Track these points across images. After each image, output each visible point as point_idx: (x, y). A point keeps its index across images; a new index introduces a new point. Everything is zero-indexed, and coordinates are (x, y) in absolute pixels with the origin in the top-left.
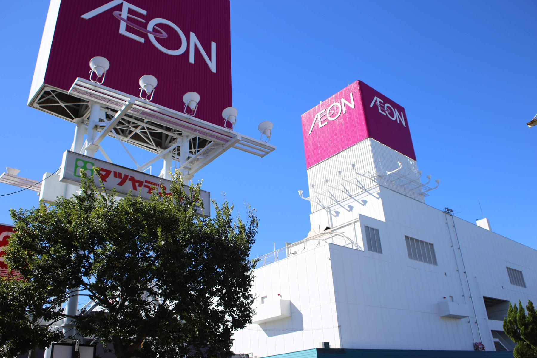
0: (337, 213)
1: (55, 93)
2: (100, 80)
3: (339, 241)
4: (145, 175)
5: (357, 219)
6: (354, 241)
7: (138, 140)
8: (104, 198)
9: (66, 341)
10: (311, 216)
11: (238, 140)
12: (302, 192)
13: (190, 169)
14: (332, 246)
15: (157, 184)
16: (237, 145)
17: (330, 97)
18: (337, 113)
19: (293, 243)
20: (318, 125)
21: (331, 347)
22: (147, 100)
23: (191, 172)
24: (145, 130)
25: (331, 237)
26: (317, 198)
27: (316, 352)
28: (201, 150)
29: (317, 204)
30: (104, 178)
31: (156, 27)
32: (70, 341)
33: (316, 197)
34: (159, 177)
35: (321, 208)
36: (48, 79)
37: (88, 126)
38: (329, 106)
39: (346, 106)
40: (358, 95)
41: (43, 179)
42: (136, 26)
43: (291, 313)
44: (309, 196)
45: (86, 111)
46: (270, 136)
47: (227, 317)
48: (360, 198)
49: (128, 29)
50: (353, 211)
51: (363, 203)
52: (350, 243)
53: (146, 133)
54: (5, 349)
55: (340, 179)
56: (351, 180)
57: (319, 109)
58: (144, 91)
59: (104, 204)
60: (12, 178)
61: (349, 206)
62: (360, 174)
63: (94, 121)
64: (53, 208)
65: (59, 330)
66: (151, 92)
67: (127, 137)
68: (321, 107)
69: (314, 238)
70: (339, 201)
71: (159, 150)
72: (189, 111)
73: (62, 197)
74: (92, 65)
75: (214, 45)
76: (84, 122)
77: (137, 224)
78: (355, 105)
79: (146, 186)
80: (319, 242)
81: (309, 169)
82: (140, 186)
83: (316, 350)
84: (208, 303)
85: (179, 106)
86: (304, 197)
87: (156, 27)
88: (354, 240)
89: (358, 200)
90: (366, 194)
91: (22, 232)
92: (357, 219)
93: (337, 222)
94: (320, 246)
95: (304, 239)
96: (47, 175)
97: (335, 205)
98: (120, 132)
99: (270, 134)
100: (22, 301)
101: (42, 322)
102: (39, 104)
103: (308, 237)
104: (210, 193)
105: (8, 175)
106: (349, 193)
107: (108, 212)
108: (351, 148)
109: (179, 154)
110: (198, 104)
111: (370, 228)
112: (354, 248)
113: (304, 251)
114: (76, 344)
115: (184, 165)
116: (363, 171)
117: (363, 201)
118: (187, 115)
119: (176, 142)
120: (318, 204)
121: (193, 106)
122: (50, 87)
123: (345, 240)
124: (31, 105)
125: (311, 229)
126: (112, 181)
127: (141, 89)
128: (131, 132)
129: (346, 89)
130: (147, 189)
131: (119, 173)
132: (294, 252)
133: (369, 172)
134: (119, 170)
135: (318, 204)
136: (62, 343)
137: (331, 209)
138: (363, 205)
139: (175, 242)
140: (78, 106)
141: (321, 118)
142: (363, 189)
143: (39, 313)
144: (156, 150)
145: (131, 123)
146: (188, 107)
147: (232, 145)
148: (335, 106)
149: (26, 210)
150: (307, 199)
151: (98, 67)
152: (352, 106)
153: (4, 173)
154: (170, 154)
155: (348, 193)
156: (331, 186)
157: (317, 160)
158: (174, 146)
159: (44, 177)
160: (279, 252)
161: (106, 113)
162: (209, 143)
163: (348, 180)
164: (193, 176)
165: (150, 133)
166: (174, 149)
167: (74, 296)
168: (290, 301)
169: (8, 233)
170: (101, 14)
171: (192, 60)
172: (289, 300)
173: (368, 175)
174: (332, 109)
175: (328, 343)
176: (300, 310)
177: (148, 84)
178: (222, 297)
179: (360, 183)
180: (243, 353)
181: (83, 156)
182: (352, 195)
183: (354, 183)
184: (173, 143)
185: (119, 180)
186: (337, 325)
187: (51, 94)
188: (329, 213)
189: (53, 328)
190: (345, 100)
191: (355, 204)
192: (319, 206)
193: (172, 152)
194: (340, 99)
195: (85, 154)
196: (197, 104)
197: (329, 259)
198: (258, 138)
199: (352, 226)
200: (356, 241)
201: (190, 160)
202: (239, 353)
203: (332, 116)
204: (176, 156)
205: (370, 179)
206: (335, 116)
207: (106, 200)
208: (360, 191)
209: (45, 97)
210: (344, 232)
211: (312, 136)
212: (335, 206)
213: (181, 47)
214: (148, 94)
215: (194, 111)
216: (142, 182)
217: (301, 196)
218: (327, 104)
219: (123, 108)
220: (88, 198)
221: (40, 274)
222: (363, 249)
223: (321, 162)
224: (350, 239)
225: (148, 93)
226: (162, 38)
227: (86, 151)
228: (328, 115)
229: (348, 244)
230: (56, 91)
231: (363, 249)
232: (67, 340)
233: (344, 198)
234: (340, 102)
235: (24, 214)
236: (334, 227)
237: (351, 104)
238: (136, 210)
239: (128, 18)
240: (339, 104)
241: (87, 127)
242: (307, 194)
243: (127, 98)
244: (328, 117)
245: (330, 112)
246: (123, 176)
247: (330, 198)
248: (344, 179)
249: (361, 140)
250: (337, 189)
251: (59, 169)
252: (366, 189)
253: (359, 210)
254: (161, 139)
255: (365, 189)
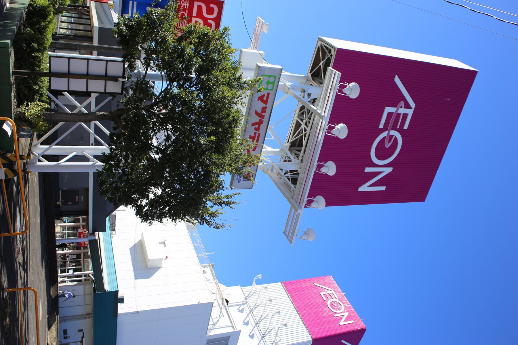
0: (242, 311)
1: (330, 57)
2: (340, 91)
3: (215, 312)
4: (265, 133)
5: (236, 329)
6: (216, 326)
7: (296, 127)
8: (239, 96)
9: (126, 72)
10: (239, 287)
11: (297, 210)
12: (261, 278)
13: (272, 171)
14: (210, 305)
15: (257, 143)
16: (293, 210)
17: (349, 301)
18: (334, 309)
19: (214, 270)
20: (322, 292)
21: (119, 305)
22: (326, 131)
23: (269, 172)
24: (305, 132)
25: (219, 304)
26: (255, 292)
27: (115, 290)
28: (290, 181)
29: (249, 292)
30: (261, 98)
31: (394, 138)
32: (126, 75)
33: (261, 302)
34: (264, 144)
35: (246, 296)
36: (341, 52)
37: (305, 84)
38: (341, 301)
39: (341, 317)
40: (352, 328)
41: (259, 51)
42: (394, 121)
43: (150, 268)
44: (257, 284)
45: (318, 83)
46: (303, 239)
47: (144, 202)
48: (256, 332)
49: (390, 114)
50: (244, 325)
51: (251, 335)
52: (214, 323)
53: (302, 133)
54: (122, 27)
55: (279, 325)
56: (272, 323)
57: (337, 292)
58: (334, 128)
59: (235, 97)
60: (260, 28)
61: (248, 322)
62: (278, 331)
63: (309, 89)
64: (232, 58)
65: (137, 67)
66: (333, 133)
67: (298, 117)
68: (339, 294)
69: (218, 288)
70: (253, 313)
71: (288, 145)
72: (319, 167)
73: (241, 66)
74: (352, 84)
75: (383, 188)
76: (308, 82)
77: (220, 123)
78: (343, 326)
79: (255, 133)
80: (214, 293)
81: (288, 295)
82: (256, 129)
83: (117, 290)
84: (156, 186)
85: (323, 158)
86: (256, 280)
87: (394, 138)
88: (217, 326)
89: (254, 330)
90: (260, 338)
91: (212, 36)
92: (236, 329)
93: (233, 311)
94: (211, 294)
95: (217, 280)
96: (262, 54)
97: (249, 309)
98: (301, 112)
99: (304, 238)
100: (157, 38)
101: (143, 56)
102: (321, 46)
103: (219, 284)
104: (252, 189)
105: (262, 25)
106: (260, 322)
107: (228, 100)
108: (302, 323)
109: (285, 161)
110: (326, 174)
111: (228, 341)
112: (209, 327)
113: (206, 279)
114: (124, 79)
115: (275, 166)
116: (280, 335)
117: (253, 334)
118: (315, 165)
119: (295, 159)
120: (250, 293)
121: (324, 170)
122: (335, 53)
123: (216, 318)
124: (319, 39)
125: (227, 287)
126: (259, 106)
127: (335, 125)
128: (302, 120)
129: (357, 317)
130: (253, 135)
131: (266, 111)
132: (206, 271)
133: (280, 340)
134: (268, 110)
135: (250, 293)
136: (125, 69)
137: (246, 305)
138: (249, 335)
139: (203, 153)
140: (321, 77)
141: (329, 294)
142: (264, 335)
143: (149, 52)
144: (288, 142)
145: (309, 120)
146: (323, 166)
147: (293, 206)
148: (341, 307)
149: (229, 39)
150: (254, 283)
151: (351, 89)
152: (342, 323)
153: (263, 21)
154: (285, 154)
155: (260, 321)
156: (261, 292)
157: (290, 291)
158: (292, 157)
159: (261, 52)
160: (205, 257)
161: (317, 99)
162: (294, 187)
163: (272, 320)
164: (266, 173)
165: (302, 137)
166: (289, 158)
167: (161, 78)
168: (161, 267)
169: (213, 26)
170: (400, 91)
171: (368, 170)
172: (162, 267)
173: (278, 339)
174: (338, 304)
175: (123, 302)
176: (153, 276)
177: (340, 130)
178: (161, 197)
179: (270, 332)
180: (116, 226)
181: (279, 82)
182: (259, 324)
183: (270, 327)
184: (294, 157)
185: (259, 112)
186: (139, 310)
187: (330, 54)
188: (241, 303)
189: (138, 63)
190: (347, 316)
191: (250, 327)
192: (248, 294)
193: (287, 156)
194: (348, 311)
195: (280, 83)
196: (326, 173)
197: (199, 303)
198: (300, 227)
199: (229, 324)
200: (216, 328)
201: (280, 171)
202: (116, 223)
203: (331, 304)
204: (284, 159)
205: (274, 341)
206: (332, 307)
207: (238, 98)
208: (262, 332)
209: (327, 50)
210: (223, 317)
211: (312, 286)
212: (248, 309)
213: (379, 160)
214: (331, 131)
215: (320, 171)
216: (258, 131)
217: (257, 277)
218: (342, 299)
219: (319, 111)
220: (240, 85)
221: (178, 50)
222: (208, 335)
223: (289, 295)
224: (218, 322)
225: (333, 131)
226: (385, 143)
227: (283, 83)
228: (332, 300)
229: (213, 321)
230: (332, 57)
231: (208, 335)
232: (127, 72)
233: (256, 317)
234: (344, 311)
235: (227, 38)
236: (229, 308)
237: (344, 322)
238: (230, 123)
239: (400, 114)
240: (342, 310)
241: (303, 84)
242: (259, 282)
243: (327, 114)
244: (331, 301)
245: (335, 302)
246: (263, 114)
247: (256, 304)
248: (280, 329)
249: (311, 333)
250: (264, 310)
251: (268, 63)
252: (265, 338)
253: (245, 331)
254: (298, 146)
255: (265, 337)
